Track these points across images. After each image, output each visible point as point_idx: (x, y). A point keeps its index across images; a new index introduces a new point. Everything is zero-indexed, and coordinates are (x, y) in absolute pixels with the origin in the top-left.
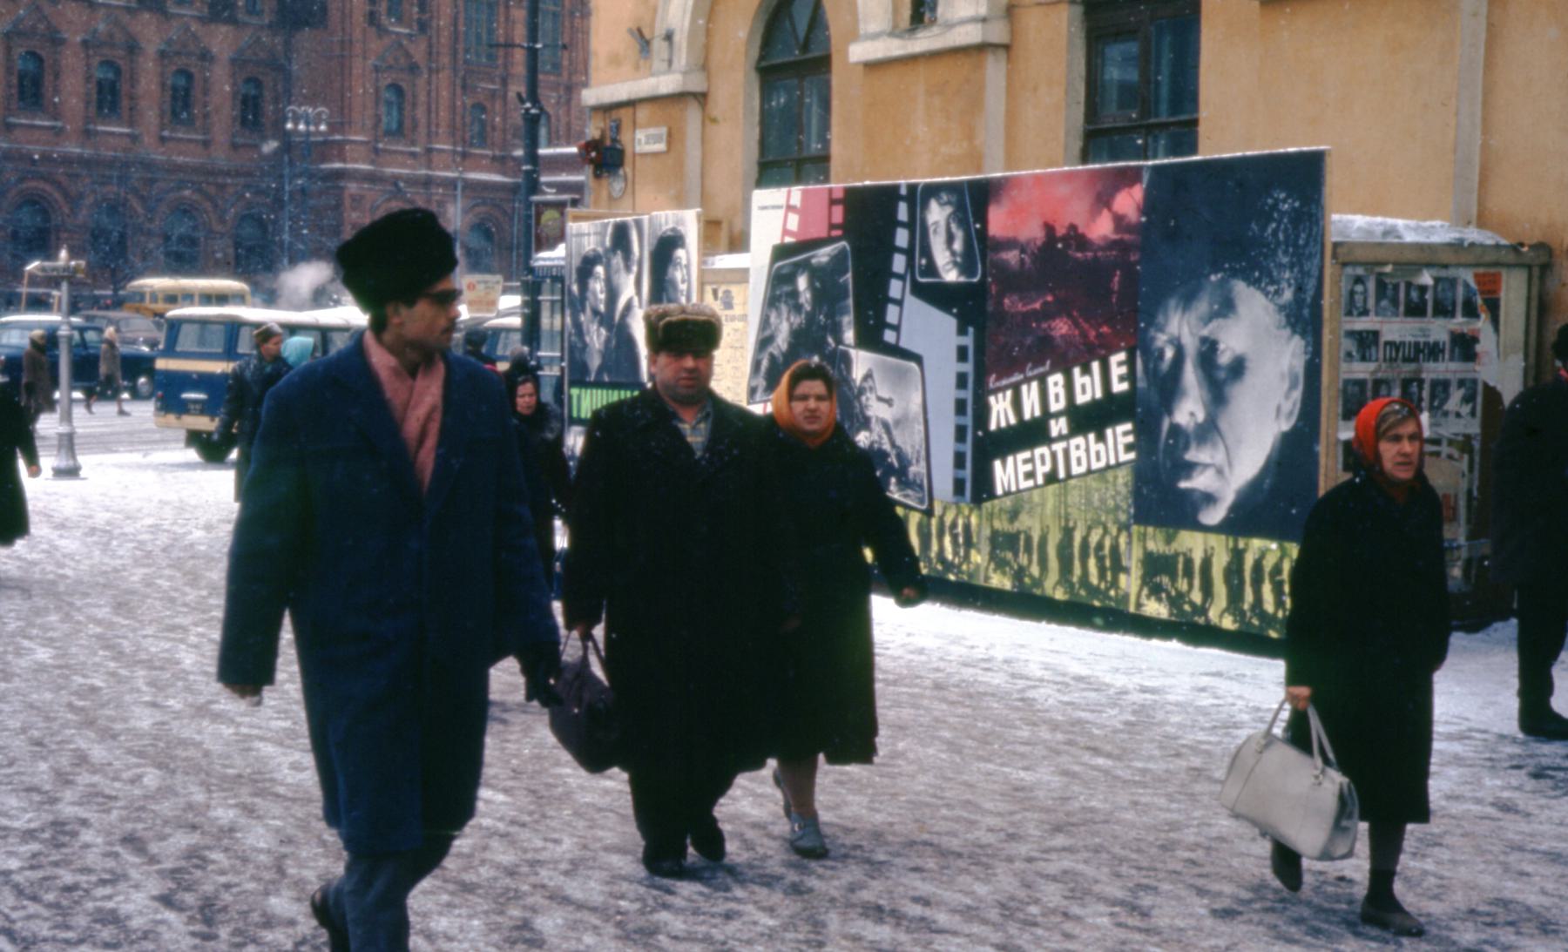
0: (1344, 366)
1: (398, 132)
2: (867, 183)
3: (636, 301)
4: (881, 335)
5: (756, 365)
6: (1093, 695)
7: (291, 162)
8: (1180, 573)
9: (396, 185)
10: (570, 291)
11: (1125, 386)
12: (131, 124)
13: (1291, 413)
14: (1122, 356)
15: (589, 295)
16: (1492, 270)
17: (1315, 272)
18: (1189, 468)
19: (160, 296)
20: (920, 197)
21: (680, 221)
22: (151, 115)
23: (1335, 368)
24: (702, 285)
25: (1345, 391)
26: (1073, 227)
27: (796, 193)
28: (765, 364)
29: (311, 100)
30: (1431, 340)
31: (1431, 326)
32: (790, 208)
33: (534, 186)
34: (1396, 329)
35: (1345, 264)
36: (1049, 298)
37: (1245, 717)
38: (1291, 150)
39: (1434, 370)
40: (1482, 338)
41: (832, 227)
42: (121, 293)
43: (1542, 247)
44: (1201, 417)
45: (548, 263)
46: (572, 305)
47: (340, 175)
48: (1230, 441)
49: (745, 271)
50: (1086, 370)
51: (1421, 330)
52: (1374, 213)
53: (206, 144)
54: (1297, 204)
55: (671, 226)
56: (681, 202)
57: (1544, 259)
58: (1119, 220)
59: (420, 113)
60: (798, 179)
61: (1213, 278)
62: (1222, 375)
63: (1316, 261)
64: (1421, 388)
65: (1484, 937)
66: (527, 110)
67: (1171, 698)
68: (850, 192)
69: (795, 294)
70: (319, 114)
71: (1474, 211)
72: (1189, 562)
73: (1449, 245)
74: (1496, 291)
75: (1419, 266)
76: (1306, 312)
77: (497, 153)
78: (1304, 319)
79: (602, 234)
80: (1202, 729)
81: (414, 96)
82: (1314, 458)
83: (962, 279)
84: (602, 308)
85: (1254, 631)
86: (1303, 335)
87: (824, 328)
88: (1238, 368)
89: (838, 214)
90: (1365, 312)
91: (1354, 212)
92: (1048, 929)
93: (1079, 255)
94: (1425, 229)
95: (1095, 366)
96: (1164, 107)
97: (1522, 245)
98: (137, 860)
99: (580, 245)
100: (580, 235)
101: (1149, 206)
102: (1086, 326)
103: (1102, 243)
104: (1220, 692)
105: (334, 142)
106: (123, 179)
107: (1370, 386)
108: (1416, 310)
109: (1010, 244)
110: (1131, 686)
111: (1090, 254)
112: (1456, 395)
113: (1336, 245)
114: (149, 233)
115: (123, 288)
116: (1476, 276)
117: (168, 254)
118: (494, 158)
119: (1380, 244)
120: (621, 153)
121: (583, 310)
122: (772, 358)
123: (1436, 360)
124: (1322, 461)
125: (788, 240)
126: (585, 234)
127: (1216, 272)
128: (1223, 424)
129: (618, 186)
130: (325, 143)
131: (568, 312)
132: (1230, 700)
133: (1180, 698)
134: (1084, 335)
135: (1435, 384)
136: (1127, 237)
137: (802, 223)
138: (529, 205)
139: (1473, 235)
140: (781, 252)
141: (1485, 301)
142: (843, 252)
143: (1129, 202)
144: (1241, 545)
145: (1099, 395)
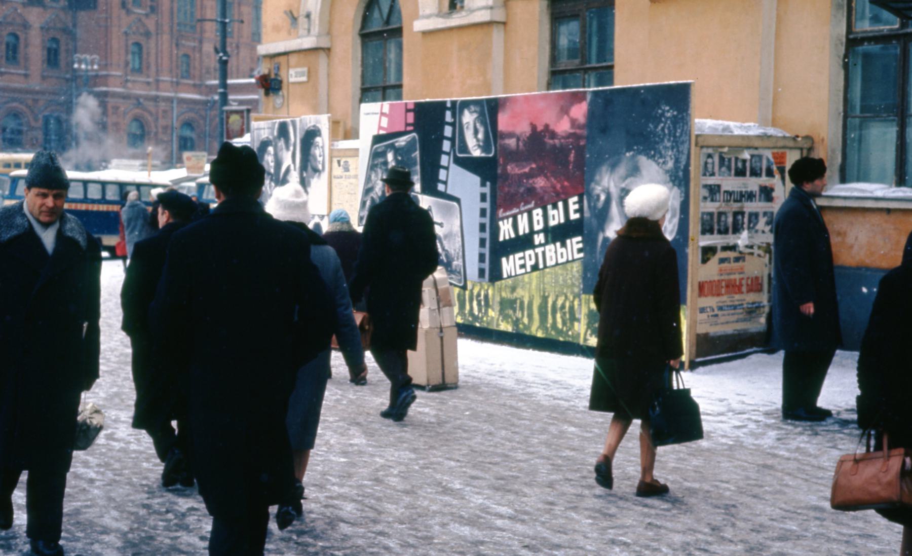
0: (702, 204)
1: (139, 71)
2: (428, 100)
3: (292, 167)
5: (363, 204)
11: (577, 216)
14: (575, 199)
17: (686, 152)
20: (458, 108)
25: (702, 218)
27: (386, 106)
28: (368, 203)
30: (749, 190)
32: (382, 114)
34: (730, 183)
35: (702, 147)
36: (534, 166)
38: (672, 82)
39: (750, 207)
40: (776, 189)
41: (407, 125)
49: (357, 150)
50: (555, 207)
52: (717, 118)
53: (26, 76)
55: (312, 124)
56: (316, 110)
58: (573, 122)
60: (384, 99)
61: (628, 154)
63: (686, 145)
64: (743, 217)
66: (221, 57)
68: (417, 105)
71: (770, 117)
72: (522, 303)
73: (758, 137)
75: (741, 148)
76: (681, 174)
77: (197, 82)
79: (272, 129)
83: (483, 155)
86: (679, 186)
89: (411, 118)
90: (713, 174)
91: (706, 118)
94: (745, 128)
95: (560, 204)
97: (797, 136)
99: (259, 135)
100: (259, 129)
101: (591, 115)
103: (564, 134)
105: (102, 76)
107: (715, 216)
108: (740, 173)
109: (511, 135)
111: (557, 141)
112: (762, 221)
113: (697, 136)
116: (773, 154)
118: (195, 86)
119: (721, 136)
120: (281, 82)
122: (373, 200)
123: (751, 201)
124: (690, 258)
125: (382, 132)
129: (279, 101)
130: (97, 76)
135: (751, 215)
137: (389, 123)
138: (222, 112)
139: (771, 131)
140: (377, 139)
141: (778, 168)
142: (414, 138)
143: (580, 111)
145: (562, 221)
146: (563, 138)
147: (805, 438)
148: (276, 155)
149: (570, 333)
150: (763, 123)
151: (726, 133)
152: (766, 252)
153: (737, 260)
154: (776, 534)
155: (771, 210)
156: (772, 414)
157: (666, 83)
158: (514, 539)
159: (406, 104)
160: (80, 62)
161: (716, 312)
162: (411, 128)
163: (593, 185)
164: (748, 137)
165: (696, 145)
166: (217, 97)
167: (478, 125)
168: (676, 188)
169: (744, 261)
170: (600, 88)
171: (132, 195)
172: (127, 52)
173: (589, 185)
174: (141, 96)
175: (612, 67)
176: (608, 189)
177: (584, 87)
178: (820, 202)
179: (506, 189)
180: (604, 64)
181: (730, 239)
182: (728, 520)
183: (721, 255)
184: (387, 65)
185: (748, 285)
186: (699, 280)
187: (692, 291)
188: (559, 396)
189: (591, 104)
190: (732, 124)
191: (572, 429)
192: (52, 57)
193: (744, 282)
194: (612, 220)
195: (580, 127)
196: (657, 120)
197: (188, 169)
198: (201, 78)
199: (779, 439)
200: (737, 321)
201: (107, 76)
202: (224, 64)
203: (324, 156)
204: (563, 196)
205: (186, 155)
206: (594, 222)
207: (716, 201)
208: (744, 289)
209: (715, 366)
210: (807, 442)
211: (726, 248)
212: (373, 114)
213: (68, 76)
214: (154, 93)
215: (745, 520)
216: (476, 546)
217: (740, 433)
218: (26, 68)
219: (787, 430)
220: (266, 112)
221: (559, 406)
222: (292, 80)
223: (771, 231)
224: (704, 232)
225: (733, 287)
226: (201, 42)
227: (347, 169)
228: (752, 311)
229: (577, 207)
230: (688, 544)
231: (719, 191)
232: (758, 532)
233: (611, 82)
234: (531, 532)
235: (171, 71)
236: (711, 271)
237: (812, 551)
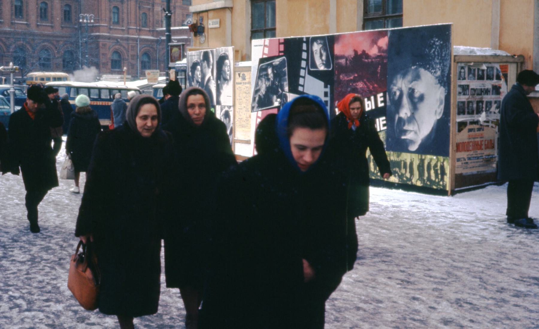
0: (458, 97)
1: (118, 23)
2: (292, 37)
3: (212, 78)
4: (298, 88)
5: (254, 99)
6: (377, 208)
7: (81, 34)
8: (402, 167)
9: (117, 40)
10: (188, 75)
11: (383, 105)
12: (27, 21)
13: (440, 113)
14: (381, 94)
15: (195, 76)
16: (505, 64)
17: (448, 65)
18: (405, 132)
19: (38, 78)
20: (310, 41)
21: (227, 51)
22: (33, 17)
23: (455, 98)
24: (235, 72)
25: (458, 105)
26: (364, 52)
27: (267, 41)
28: (257, 99)
29: (88, 12)
30: (486, 88)
31: (486, 83)
32: (265, 46)
33: (169, 39)
34: (475, 84)
35: (458, 63)
36: (356, 75)
37: (430, 215)
38: (439, 24)
39: (487, 98)
40: (502, 87)
41: (280, 52)
42: (25, 77)
43: (521, 56)
44: (409, 114)
45: (180, 65)
46: (189, 79)
47: (98, 37)
48: (419, 123)
49: (250, 67)
50: (369, 99)
51: (483, 84)
52: (466, 45)
53: (52, 27)
54: (442, 42)
55: (223, 52)
56: (225, 44)
57: (522, 60)
58: (380, 49)
59: (125, 16)
60: (265, 37)
61: (413, 68)
62: (416, 100)
63: (448, 61)
64: (483, 104)
65: (528, 289)
66: (167, 14)
67: (404, 209)
68: (285, 40)
69: (267, 75)
70: (91, 16)
71: (498, 44)
72: (405, 164)
73: (491, 56)
74: (506, 71)
75: (482, 63)
76: (445, 79)
77: (151, 29)
78: (445, 81)
79: (200, 55)
80: (416, 220)
81: (123, 10)
82: (448, 128)
83: (326, 69)
84: (200, 80)
85: (428, 186)
86: (444, 86)
87: (277, 86)
88: (422, 98)
89: (282, 48)
90: (464, 79)
91: (460, 45)
92: (381, 290)
93: (366, 60)
94: (484, 50)
95: (372, 98)
96: (390, 10)
97: (515, 55)
98: (63, 271)
99: (192, 59)
100: (191, 56)
101: (391, 44)
102: (369, 84)
103: (374, 56)
104: (419, 207)
105: (96, 26)
106: (24, 39)
107: (466, 104)
108: (481, 78)
109: (342, 57)
110: (389, 206)
111: (370, 60)
112: (494, 106)
113: (455, 56)
114: (33, 57)
115: (26, 75)
116: (500, 66)
117: (40, 64)
118: (150, 31)
119: (469, 56)
120: (204, 28)
121: (193, 81)
122: (260, 96)
123: (487, 94)
124: (451, 129)
125: (265, 56)
126: (193, 55)
127: (414, 66)
128: (417, 116)
129: (203, 39)
130: (93, 26)
131: (188, 82)
132: (424, 210)
133: (407, 209)
134: (368, 87)
135: (487, 102)
136: (382, 54)
137: (269, 51)
138: (168, 46)
139: (499, 52)
140: (262, 61)
141: (503, 75)
142: (284, 60)
143: (383, 42)
144: (423, 157)
145: (374, 108)
146: (374, 58)
147: (524, 235)
148: (202, 71)
149: (441, 183)
150: (494, 47)
151: (472, 54)
152: (496, 125)
153: (479, 130)
154: (512, 294)
155: (499, 100)
156: (503, 221)
157: (436, 24)
158: (354, 297)
159: (279, 40)
160: (83, 18)
161: (467, 161)
162: (282, 54)
163: (392, 86)
164: (486, 57)
165: (455, 61)
166: (164, 38)
167: (322, 51)
168: (442, 88)
169: (483, 130)
170: (396, 28)
171: (117, 95)
172: (110, 12)
173: (390, 86)
174: (118, 38)
175: (402, 16)
176: (401, 88)
177: (385, 28)
178: (532, 95)
179: (340, 89)
180: (397, 14)
181: (475, 117)
182: (482, 286)
183: (469, 127)
184: (267, 16)
185: (485, 145)
186: (457, 142)
187: (453, 148)
188: (374, 211)
189: (390, 39)
190: (475, 48)
191: (384, 231)
192: (67, 15)
193: (483, 143)
194: (403, 107)
195: (383, 51)
196: (431, 47)
197: (148, 80)
198: (153, 26)
199: (508, 237)
200: (479, 166)
201: (99, 26)
202: (168, 18)
203: (230, 71)
204: (374, 93)
205: (147, 72)
206: (393, 108)
207: (466, 95)
208: (483, 147)
209: (466, 193)
210: (526, 238)
211: (473, 123)
212: (260, 46)
213: (76, 27)
214: (126, 36)
215: (492, 285)
216: (333, 301)
217: (486, 233)
218: (52, 23)
219: (512, 231)
220: (195, 45)
221: (375, 218)
222: (210, 26)
223: (499, 112)
224: (459, 114)
225: (478, 146)
226: (153, 6)
227: (244, 79)
228: (488, 161)
229: (382, 99)
230: (459, 300)
231: (468, 89)
232: (501, 292)
233: (401, 25)
234: (364, 293)
235: (136, 23)
236: (463, 136)
237: (535, 304)
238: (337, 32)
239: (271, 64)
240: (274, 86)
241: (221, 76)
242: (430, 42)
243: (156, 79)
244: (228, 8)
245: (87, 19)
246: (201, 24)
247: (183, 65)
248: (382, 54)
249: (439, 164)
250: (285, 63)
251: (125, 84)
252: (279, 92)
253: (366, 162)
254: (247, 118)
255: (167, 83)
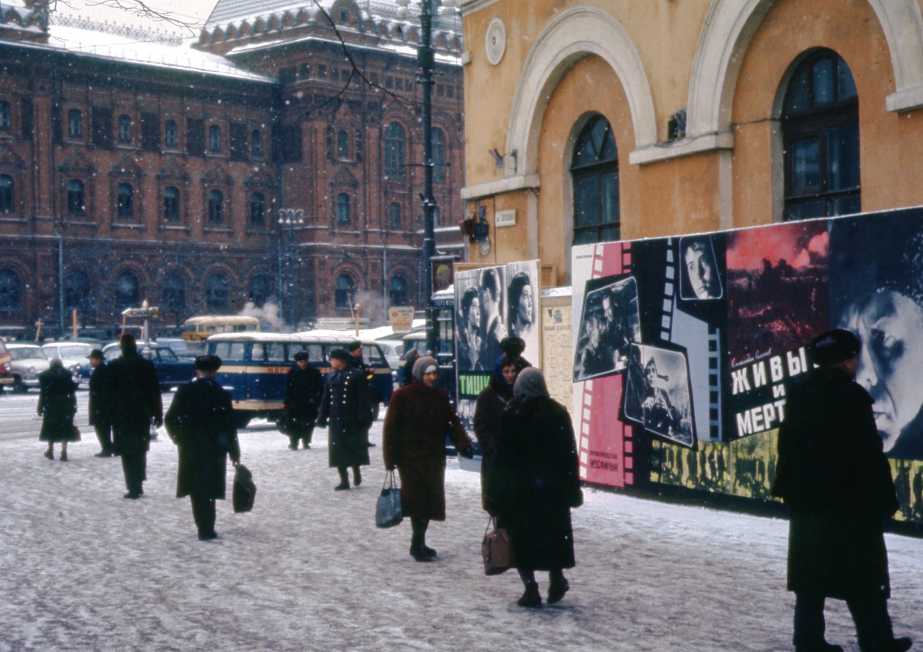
2: (646, 239)
4: (659, 335)
5: (578, 357)
9: (346, 254)
10: (458, 315)
15: (470, 316)
20: (680, 246)
24: (542, 307)
26: (783, 262)
27: (600, 247)
28: (584, 356)
32: (596, 257)
33: (431, 250)
36: (769, 308)
41: (624, 267)
42: (182, 326)
44: (874, 382)
46: (459, 322)
47: (313, 249)
48: (894, 397)
49: (569, 297)
50: (796, 354)
55: (520, 271)
56: (526, 256)
58: (813, 256)
60: (600, 239)
61: (879, 291)
62: (888, 354)
66: (426, 204)
68: (634, 244)
69: (602, 311)
77: (408, 232)
79: (477, 278)
83: (711, 298)
84: (478, 324)
87: (621, 333)
88: (899, 349)
93: (788, 279)
96: (837, 182)
99: (463, 286)
100: (463, 279)
101: (833, 245)
109: (742, 274)
115: (183, 323)
117: (209, 302)
120: (487, 227)
121: (466, 326)
125: (596, 277)
126: (466, 278)
127: (880, 287)
128: (890, 386)
129: (486, 247)
130: (302, 231)
132: (906, 569)
134: (793, 331)
136: (818, 266)
137: (605, 265)
140: (592, 285)
142: (632, 282)
143: (820, 243)
146: (801, 274)
159: (622, 244)
160: (285, 217)
167: (703, 264)
177: (826, 215)
179: (739, 336)
220: (472, 259)
227: (559, 320)
238: (735, 225)
239: (609, 290)
240: (615, 332)
241: (516, 315)
242: (912, 241)
243: (408, 324)
244: (531, 189)
245: (291, 218)
246: (482, 219)
247: (448, 297)
248: (818, 266)
249: (716, 454)
250: (634, 289)
251: (357, 334)
252: (624, 342)
253: (373, 417)
254: (566, 393)
255: (427, 331)
